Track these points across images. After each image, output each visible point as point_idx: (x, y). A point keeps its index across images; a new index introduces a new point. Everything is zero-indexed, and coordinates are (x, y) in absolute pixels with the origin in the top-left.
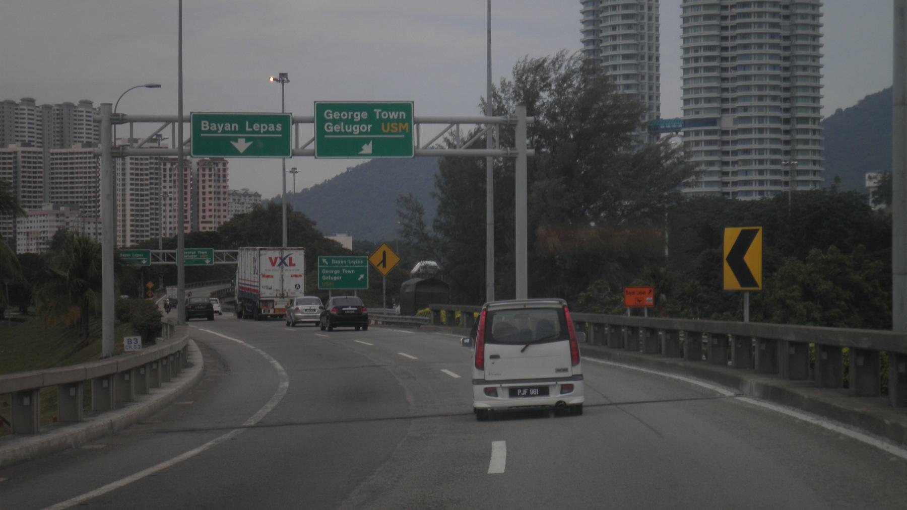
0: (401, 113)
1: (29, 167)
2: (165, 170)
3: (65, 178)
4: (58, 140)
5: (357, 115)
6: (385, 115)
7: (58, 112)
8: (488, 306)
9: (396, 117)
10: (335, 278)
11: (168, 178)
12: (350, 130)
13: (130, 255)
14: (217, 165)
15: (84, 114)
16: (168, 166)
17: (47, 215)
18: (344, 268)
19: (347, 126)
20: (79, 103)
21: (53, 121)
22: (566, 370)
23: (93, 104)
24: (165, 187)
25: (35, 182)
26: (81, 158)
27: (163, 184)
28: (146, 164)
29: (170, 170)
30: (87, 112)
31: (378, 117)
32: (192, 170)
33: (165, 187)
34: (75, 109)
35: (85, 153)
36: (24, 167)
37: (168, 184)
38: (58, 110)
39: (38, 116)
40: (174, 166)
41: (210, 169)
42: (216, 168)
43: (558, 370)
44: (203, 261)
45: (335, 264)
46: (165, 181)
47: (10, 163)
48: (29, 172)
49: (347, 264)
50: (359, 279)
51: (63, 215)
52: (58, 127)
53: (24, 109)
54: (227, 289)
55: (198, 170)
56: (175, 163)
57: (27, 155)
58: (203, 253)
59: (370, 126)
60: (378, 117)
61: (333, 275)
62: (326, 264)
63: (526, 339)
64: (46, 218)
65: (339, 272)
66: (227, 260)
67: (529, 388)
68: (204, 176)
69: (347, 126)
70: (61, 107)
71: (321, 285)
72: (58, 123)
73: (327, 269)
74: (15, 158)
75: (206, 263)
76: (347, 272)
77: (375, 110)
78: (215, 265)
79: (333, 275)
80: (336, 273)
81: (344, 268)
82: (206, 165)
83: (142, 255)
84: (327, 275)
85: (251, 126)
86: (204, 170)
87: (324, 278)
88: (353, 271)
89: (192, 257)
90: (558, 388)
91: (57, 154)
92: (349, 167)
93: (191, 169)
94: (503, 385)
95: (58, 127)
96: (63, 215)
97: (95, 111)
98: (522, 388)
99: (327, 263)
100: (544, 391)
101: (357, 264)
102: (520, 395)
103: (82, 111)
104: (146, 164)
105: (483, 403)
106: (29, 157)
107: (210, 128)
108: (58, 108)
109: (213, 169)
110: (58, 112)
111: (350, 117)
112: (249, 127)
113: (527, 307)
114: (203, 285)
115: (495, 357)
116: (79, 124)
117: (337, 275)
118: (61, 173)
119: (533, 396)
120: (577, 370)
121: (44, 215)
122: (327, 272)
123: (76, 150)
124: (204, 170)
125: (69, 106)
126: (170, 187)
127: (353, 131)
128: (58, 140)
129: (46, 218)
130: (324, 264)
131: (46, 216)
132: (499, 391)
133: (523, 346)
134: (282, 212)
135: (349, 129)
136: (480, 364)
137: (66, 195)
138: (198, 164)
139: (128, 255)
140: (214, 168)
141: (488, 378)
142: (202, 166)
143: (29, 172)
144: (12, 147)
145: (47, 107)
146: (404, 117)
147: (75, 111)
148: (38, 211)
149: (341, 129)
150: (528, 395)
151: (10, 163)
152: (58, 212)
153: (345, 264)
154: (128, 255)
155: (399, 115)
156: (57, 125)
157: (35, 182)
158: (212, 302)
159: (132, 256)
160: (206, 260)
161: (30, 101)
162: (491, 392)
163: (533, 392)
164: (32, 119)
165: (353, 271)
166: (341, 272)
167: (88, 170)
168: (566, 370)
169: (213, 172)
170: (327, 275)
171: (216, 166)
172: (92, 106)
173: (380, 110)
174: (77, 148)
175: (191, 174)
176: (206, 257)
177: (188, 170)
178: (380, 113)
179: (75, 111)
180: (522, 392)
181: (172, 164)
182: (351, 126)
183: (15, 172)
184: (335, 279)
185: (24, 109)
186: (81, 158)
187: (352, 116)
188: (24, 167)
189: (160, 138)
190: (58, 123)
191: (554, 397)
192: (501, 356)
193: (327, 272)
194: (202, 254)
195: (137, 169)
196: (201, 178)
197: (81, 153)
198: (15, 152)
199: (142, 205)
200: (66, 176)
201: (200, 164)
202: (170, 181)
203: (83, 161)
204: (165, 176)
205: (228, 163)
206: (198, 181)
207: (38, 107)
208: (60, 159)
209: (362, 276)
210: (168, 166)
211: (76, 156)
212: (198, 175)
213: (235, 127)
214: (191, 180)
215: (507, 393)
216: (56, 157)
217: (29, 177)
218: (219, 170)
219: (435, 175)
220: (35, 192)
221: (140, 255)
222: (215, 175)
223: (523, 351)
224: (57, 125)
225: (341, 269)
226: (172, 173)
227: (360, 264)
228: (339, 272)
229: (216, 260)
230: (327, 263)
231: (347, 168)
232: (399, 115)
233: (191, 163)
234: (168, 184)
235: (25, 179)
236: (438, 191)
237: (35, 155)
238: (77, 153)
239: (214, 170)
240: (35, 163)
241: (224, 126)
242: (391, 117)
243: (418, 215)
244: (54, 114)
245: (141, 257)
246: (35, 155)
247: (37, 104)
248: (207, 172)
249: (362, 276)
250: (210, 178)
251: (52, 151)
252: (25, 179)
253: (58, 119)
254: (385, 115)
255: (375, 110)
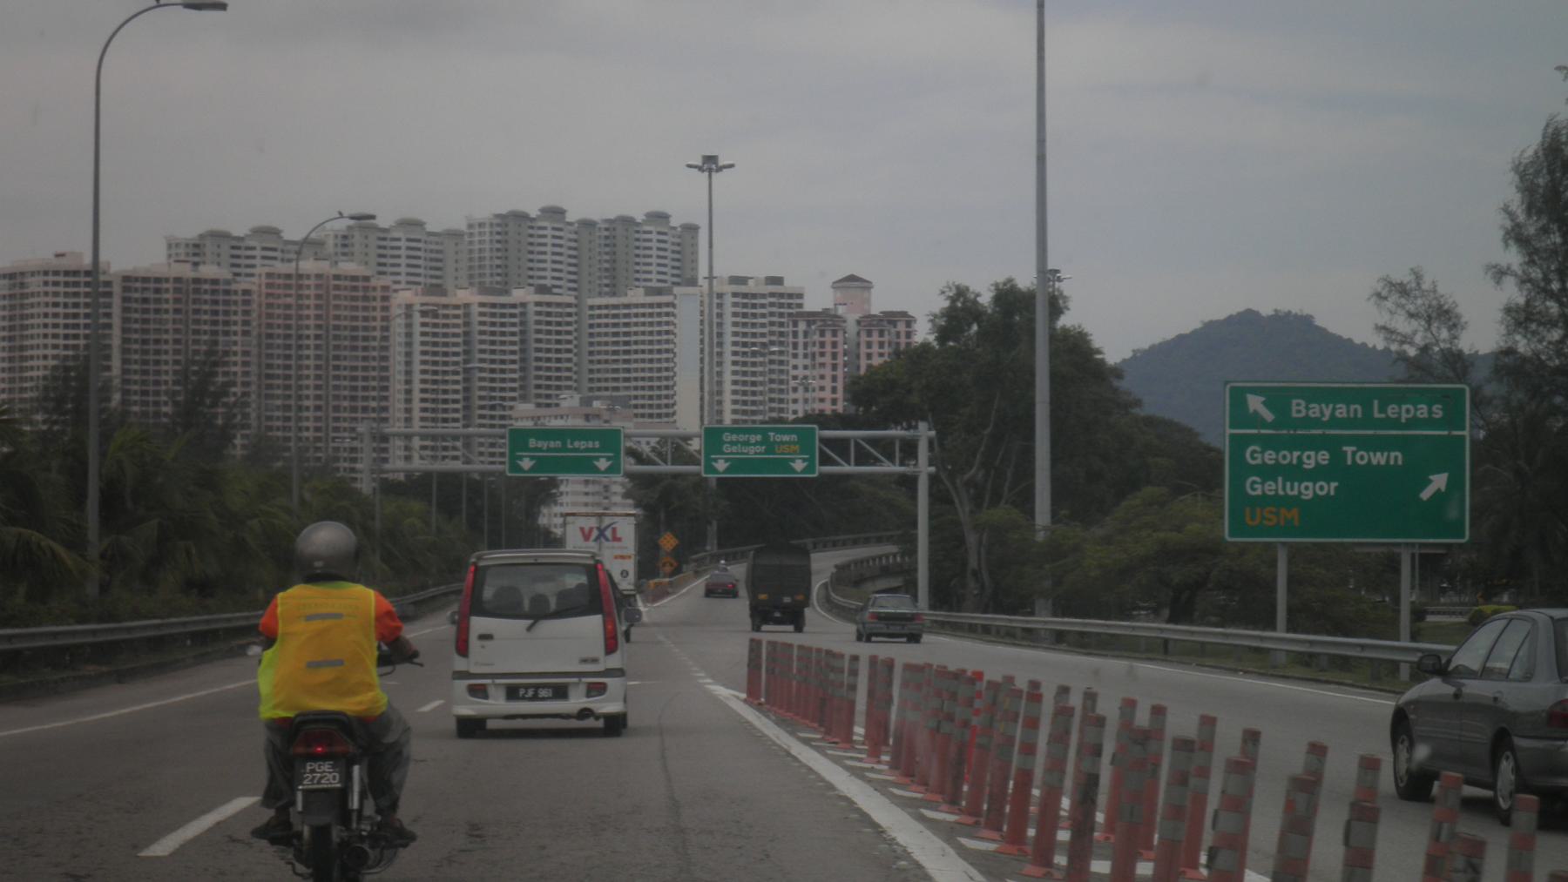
0: (1393, 454)
1: (549, 332)
2: (795, 334)
3: (615, 353)
4: (607, 285)
5: (1309, 457)
6: (1362, 458)
7: (606, 233)
8: (480, 558)
9: (1383, 462)
10: (1308, 490)
11: (800, 351)
12: (1295, 492)
13: (559, 443)
14: (895, 327)
15: (654, 236)
16: (802, 326)
17: (568, 416)
18: (1350, 440)
19: (1288, 484)
20: (644, 218)
21: (598, 250)
22: (595, 661)
23: (671, 219)
24: (795, 367)
25: (559, 360)
26: (644, 315)
27: (793, 362)
28: (763, 325)
29: (806, 334)
30: (659, 233)
31: (1349, 462)
32: (847, 335)
33: (795, 367)
34: (638, 229)
35: (651, 305)
36: (538, 332)
37: (800, 362)
38: (607, 229)
39: (570, 240)
40: (813, 327)
41: (881, 334)
42: (893, 330)
43: (585, 661)
44: (785, 465)
45: (1308, 422)
46: (795, 356)
47: (513, 325)
48: (549, 341)
49: (1368, 421)
50: (1426, 495)
51: (598, 416)
52: (607, 261)
53: (545, 228)
54: (880, 557)
55: (858, 334)
56: (814, 322)
57: (545, 309)
58: (786, 438)
59: (1334, 485)
60: (1349, 462)
61: (1296, 473)
62: (1263, 420)
63: (539, 613)
64: (566, 421)
65: (1324, 457)
66: (857, 464)
67: (537, 687)
68: (869, 345)
69: (1288, 484)
70: (612, 224)
71: (1238, 527)
72: (607, 253)
73: (1268, 443)
74: (523, 314)
75: (793, 471)
76: (1363, 458)
77: (1345, 448)
78: (822, 475)
79: (1296, 473)
80: (1310, 464)
81: (1350, 440)
82: (874, 326)
83: (597, 444)
84: (1268, 473)
85: (1382, 409)
86: (869, 334)
87: (1256, 487)
88: (1396, 457)
89: (752, 449)
90: (582, 689)
91: (600, 307)
92: (1136, 348)
93: (845, 332)
94: (498, 681)
95: (607, 261)
96: (598, 416)
97: (673, 232)
98: (527, 687)
99: (1268, 416)
100: (561, 692)
101: (1414, 423)
102: (524, 698)
103: (650, 232)
104: (763, 325)
105: (469, 708)
106: (549, 314)
107: (726, 442)
108: (607, 226)
109: (886, 333)
110: (606, 233)
111: (1295, 462)
112: (1380, 412)
113: (539, 561)
114: (825, 546)
115: (485, 637)
116: (645, 256)
117: (1317, 474)
118: (606, 344)
119: (543, 699)
120: (614, 661)
121: (562, 417)
122: (1269, 457)
123: (634, 301)
124: (869, 334)
125: (627, 221)
126: (806, 367)
127: (1300, 493)
128: (607, 285)
129: (566, 421)
130: (1257, 421)
131: (565, 417)
132: (491, 691)
133: (529, 622)
134: (1034, 312)
135: (1292, 489)
136: (462, 648)
137: (615, 384)
138: (858, 322)
139: (552, 444)
140: (889, 332)
141: (474, 670)
142: (865, 326)
143: (549, 341)
144: (518, 295)
145: (588, 224)
146: (1359, 415)
147: (638, 232)
148: (553, 410)
149: (1276, 490)
150: (535, 698)
151: (513, 325)
152: (588, 410)
153: (1350, 423)
154: (552, 444)
155: (1388, 457)
156: (607, 257)
157: (559, 360)
158: (1396, 550)
159: (975, 574)
160: (793, 460)
161: (555, 213)
162: (478, 691)
163: (543, 693)
164: (560, 246)
165: (1396, 457)
166: (1337, 456)
167: (656, 338)
168: (595, 661)
169: (886, 338)
170: (1268, 473)
171: (892, 326)
172: (669, 222)
173: (1354, 448)
174: (637, 296)
175: (845, 343)
176: (795, 452)
177: (840, 334)
178: (1354, 453)
179: (638, 232)
180: (526, 693)
181: (809, 324)
182: (1296, 484)
183: (523, 342)
184: (1308, 495)
185: (545, 228)
186: (644, 315)
187: (1299, 458)
188: (538, 332)
189: (714, 166)
190: (607, 253)
191: (576, 701)
192: (495, 637)
193: (1269, 457)
194: (782, 443)
195: (745, 335)
196: (863, 350)
197: (643, 306)
198: (523, 305)
199: (754, 403)
200: (616, 348)
201: (863, 324)
202: (805, 356)
203: (648, 329)
204: (795, 345)
205: (915, 321)
206: (858, 357)
207: (570, 224)
208: (606, 316)
209: (1439, 481)
210: (802, 326)
211: (635, 311)
212: (858, 344)
213: (1356, 410)
214: (845, 355)
215: (502, 693)
216: (598, 312)
217: (548, 351)
218: (898, 334)
219: (1506, 210)
220: (558, 378)
221: (590, 444)
222: (890, 344)
223: (529, 629)
224: (607, 257)
225: (1333, 445)
226: (808, 340)
227: (1430, 422)
228: (1324, 457)
229: (825, 460)
230: (1268, 416)
231: (1134, 351)
232: (1388, 457)
233: (845, 321)
234: (800, 362)
235: (540, 364)
236: (1513, 257)
237: (560, 310)
238: (637, 306)
239: (889, 334)
240: (559, 324)
241: (1334, 409)
242: (1374, 462)
243: (1444, 334)
244: (600, 237)
245: (593, 450)
246: (560, 310)
247: (570, 217)
248: (875, 338)
249: (1439, 481)
250: (881, 351)
251: (590, 302)
252: (540, 364)
253: (606, 245)
254: (1362, 458)
255: (1345, 448)
